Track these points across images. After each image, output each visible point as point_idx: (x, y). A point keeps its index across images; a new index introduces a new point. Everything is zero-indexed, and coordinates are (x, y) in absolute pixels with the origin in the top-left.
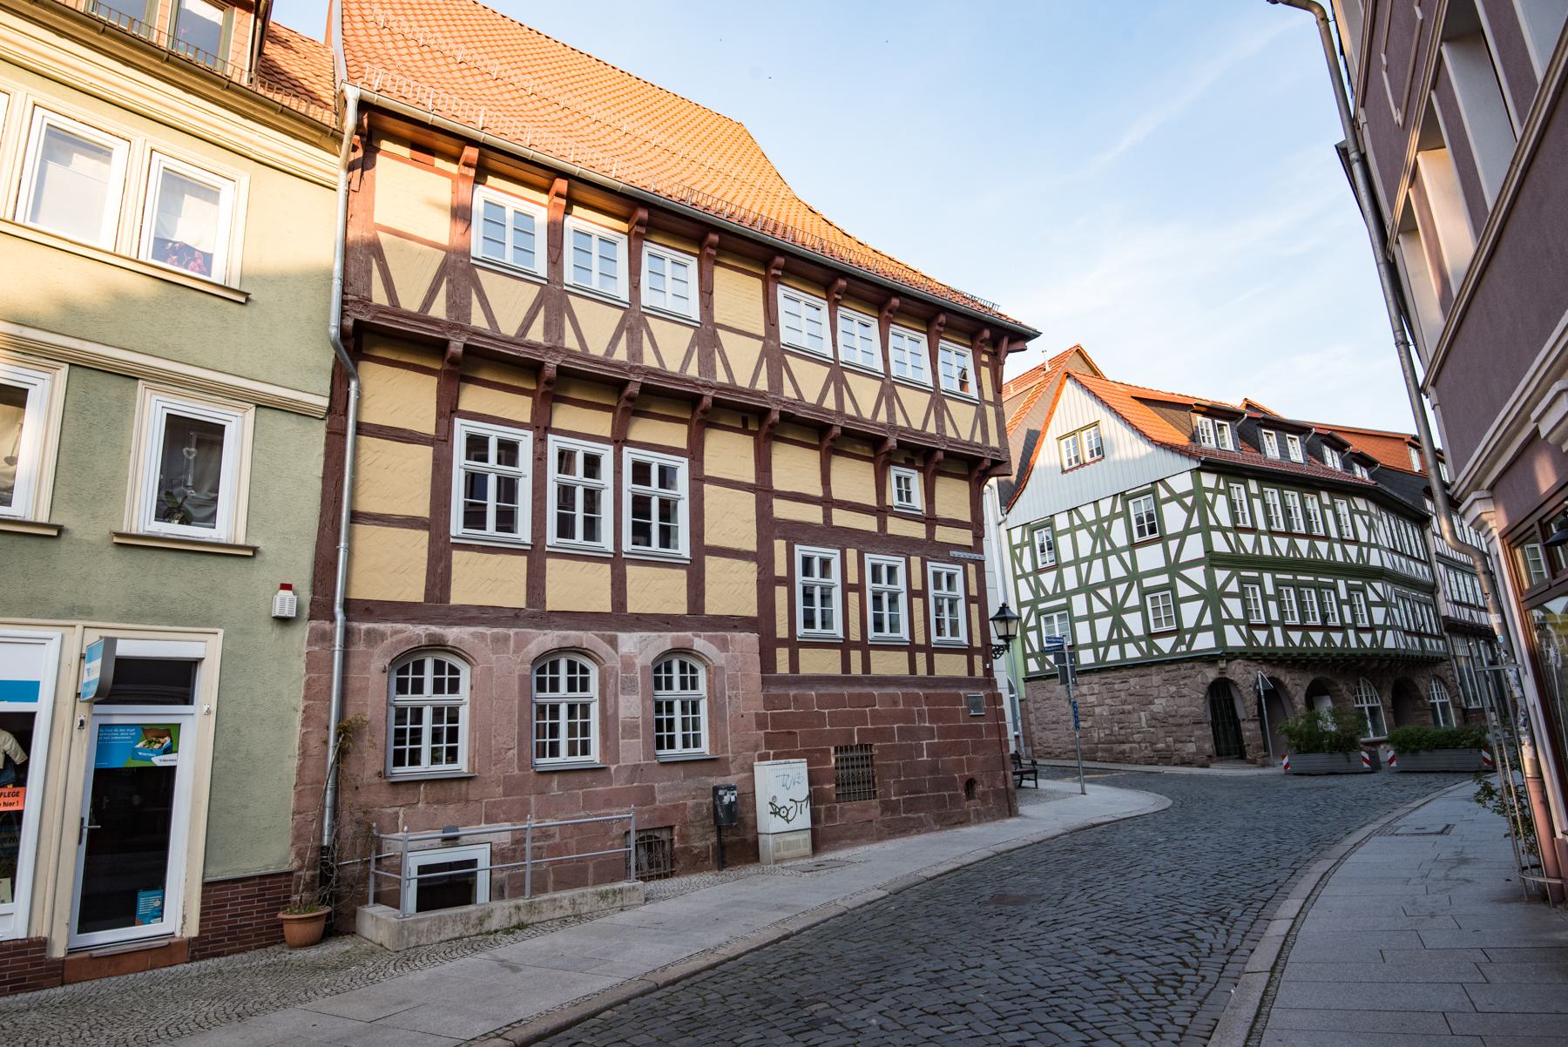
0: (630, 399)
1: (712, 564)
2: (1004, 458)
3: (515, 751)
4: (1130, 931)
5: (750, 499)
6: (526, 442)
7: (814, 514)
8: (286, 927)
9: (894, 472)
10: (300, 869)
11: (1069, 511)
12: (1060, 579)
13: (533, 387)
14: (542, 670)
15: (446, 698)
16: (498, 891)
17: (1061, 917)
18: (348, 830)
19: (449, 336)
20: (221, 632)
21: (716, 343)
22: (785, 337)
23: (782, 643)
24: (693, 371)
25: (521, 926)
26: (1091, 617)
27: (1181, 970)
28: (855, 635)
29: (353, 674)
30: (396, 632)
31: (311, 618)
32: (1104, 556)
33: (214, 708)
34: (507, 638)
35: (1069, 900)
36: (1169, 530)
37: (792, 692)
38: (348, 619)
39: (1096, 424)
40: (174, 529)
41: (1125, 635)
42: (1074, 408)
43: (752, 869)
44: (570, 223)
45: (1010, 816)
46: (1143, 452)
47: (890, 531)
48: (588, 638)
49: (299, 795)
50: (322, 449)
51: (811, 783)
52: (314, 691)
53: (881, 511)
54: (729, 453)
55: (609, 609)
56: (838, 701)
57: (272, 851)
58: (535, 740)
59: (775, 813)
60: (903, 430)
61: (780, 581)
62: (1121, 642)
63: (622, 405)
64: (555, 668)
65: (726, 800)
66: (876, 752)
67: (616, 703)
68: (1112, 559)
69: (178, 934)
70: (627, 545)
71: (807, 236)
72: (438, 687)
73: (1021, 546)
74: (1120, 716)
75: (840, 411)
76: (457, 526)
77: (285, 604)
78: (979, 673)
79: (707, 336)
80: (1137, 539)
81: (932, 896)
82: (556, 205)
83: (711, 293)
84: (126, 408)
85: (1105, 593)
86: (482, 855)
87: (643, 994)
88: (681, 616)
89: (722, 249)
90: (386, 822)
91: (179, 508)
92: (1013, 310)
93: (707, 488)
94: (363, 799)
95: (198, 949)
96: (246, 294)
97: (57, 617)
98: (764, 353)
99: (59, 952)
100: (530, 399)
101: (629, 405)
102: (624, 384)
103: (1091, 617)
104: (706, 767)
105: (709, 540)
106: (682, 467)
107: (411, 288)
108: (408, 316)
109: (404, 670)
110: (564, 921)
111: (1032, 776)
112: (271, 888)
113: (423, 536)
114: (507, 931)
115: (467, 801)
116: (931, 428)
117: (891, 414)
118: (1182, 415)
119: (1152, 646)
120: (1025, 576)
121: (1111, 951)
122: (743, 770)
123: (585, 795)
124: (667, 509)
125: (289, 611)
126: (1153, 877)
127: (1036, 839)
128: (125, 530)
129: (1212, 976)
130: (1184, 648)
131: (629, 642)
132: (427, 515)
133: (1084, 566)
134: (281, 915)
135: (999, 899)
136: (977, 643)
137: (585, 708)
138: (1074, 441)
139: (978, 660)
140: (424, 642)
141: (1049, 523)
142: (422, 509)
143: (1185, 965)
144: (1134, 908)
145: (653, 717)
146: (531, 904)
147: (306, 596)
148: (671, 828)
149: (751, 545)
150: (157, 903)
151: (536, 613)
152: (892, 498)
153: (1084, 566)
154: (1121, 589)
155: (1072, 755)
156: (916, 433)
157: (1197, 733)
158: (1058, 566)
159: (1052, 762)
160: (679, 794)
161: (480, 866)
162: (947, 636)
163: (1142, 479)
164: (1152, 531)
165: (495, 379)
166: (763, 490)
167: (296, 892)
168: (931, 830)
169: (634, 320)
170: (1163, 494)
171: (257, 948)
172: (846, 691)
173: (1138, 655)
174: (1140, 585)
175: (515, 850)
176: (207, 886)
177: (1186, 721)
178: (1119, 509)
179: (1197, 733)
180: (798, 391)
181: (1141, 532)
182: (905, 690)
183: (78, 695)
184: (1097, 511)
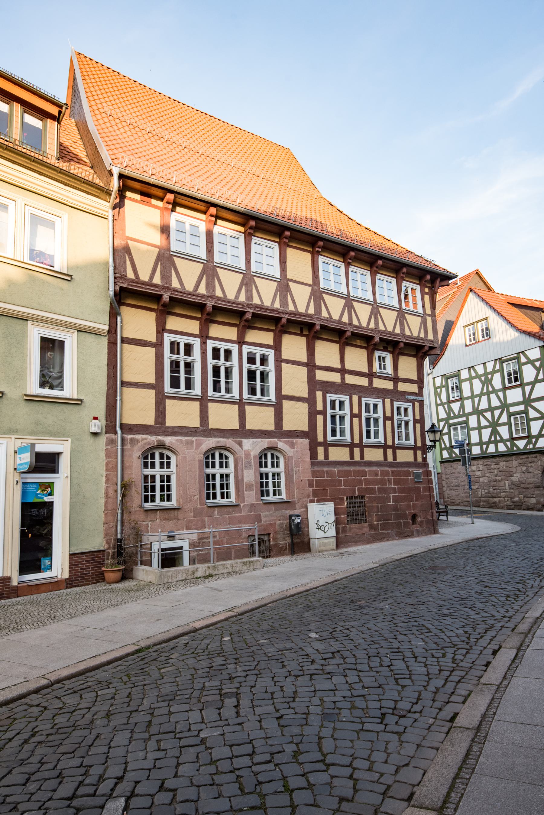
0: (247, 321)
1: (286, 404)
3: (198, 496)
4: (496, 579)
5: (304, 371)
6: (197, 343)
7: (336, 378)
8: (106, 575)
9: (377, 354)
10: (109, 548)
11: (469, 368)
12: (462, 407)
13: (200, 316)
14: (207, 458)
15: (165, 471)
16: (192, 561)
17: (463, 574)
18: (127, 532)
19: (162, 293)
20: (70, 440)
21: (288, 289)
22: (322, 284)
23: (320, 444)
24: (277, 305)
25: (210, 576)
26: (480, 428)
27: (518, 593)
28: (357, 440)
29: (126, 459)
30: (143, 439)
31: (106, 433)
32: (488, 394)
33: (69, 475)
35: (467, 568)
36: (526, 381)
37: (325, 469)
38: (122, 433)
39: (486, 319)
40: (46, 392)
41: (498, 438)
42: (474, 309)
43: (308, 555)
44: (217, 229)
45: (434, 533)
46: (513, 337)
48: (228, 442)
49: (106, 515)
50: (106, 351)
51: (335, 515)
52: (110, 467)
53: (371, 375)
54: (294, 346)
55: (238, 428)
57: (96, 541)
58: (143, 494)
60: (383, 332)
61: (320, 413)
62: (496, 442)
63: (242, 324)
64: (266, 456)
65: (296, 521)
66: (367, 500)
67: (243, 474)
68: (493, 396)
69: (59, 577)
70: (246, 395)
71: (332, 228)
72: (162, 465)
73: (440, 387)
74: (493, 483)
75: (350, 324)
76: (167, 388)
77: (96, 426)
78: (420, 460)
79: (284, 286)
80: (507, 385)
81: (401, 567)
82: (210, 221)
83: (285, 263)
84: (24, 334)
85: (488, 415)
86: (185, 544)
87: (282, 599)
88: (271, 431)
89: (291, 238)
90: (143, 528)
91: (48, 382)
92: (443, 261)
93: (284, 365)
94: (133, 517)
95: (70, 583)
96: (71, 276)
97: (4, 434)
98: (313, 293)
99: (15, 583)
100: (198, 322)
101: (246, 324)
102: (243, 313)
103: (480, 428)
104: (285, 505)
105: (151, 352)
106: (271, 355)
107: (145, 270)
108: (144, 283)
109: (146, 457)
110: (229, 574)
111: (445, 514)
112: (96, 557)
113: (153, 392)
114: (205, 577)
115: (178, 519)
116: (398, 331)
117: (377, 324)
118: (536, 314)
119: (513, 445)
120: (442, 404)
121: (487, 586)
122: (303, 507)
123: (230, 518)
124: (264, 376)
125: (98, 430)
126: (508, 560)
127: (449, 544)
128: (28, 393)
129: (531, 595)
130: (531, 446)
131: (248, 443)
132: (154, 382)
133: (476, 400)
134: (103, 569)
135: (433, 568)
136: (419, 444)
137: (227, 476)
138: (473, 328)
139: (419, 453)
141: (457, 375)
142: (151, 379)
143: (520, 591)
144: (498, 571)
145: (259, 481)
146: (214, 566)
147: (104, 422)
148: (269, 534)
149: (305, 395)
150: (49, 563)
151: (203, 429)
152: (376, 368)
153: (476, 400)
154: (497, 413)
155: (466, 504)
156: (390, 333)
157: (537, 492)
158: (461, 399)
159: (455, 508)
160: (274, 518)
161: (184, 549)
162: (404, 441)
163: (512, 352)
164: (516, 379)
165: (182, 313)
166: (311, 365)
167: (108, 559)
168: (394, 539)
169: (248, 280)
170: (523, 359)
171: (92, 583)
172: (352, 468)
173: (505, 449)
174: (508, 410)
175: (199, 543)
176: (71, 555)
177: (531, 486)
178: (497, 367)
179: (537, 492)
180: (329, 313)
181: (510, 381)
182: (382, 468)
183: (15, 469)
184: (485, 368)
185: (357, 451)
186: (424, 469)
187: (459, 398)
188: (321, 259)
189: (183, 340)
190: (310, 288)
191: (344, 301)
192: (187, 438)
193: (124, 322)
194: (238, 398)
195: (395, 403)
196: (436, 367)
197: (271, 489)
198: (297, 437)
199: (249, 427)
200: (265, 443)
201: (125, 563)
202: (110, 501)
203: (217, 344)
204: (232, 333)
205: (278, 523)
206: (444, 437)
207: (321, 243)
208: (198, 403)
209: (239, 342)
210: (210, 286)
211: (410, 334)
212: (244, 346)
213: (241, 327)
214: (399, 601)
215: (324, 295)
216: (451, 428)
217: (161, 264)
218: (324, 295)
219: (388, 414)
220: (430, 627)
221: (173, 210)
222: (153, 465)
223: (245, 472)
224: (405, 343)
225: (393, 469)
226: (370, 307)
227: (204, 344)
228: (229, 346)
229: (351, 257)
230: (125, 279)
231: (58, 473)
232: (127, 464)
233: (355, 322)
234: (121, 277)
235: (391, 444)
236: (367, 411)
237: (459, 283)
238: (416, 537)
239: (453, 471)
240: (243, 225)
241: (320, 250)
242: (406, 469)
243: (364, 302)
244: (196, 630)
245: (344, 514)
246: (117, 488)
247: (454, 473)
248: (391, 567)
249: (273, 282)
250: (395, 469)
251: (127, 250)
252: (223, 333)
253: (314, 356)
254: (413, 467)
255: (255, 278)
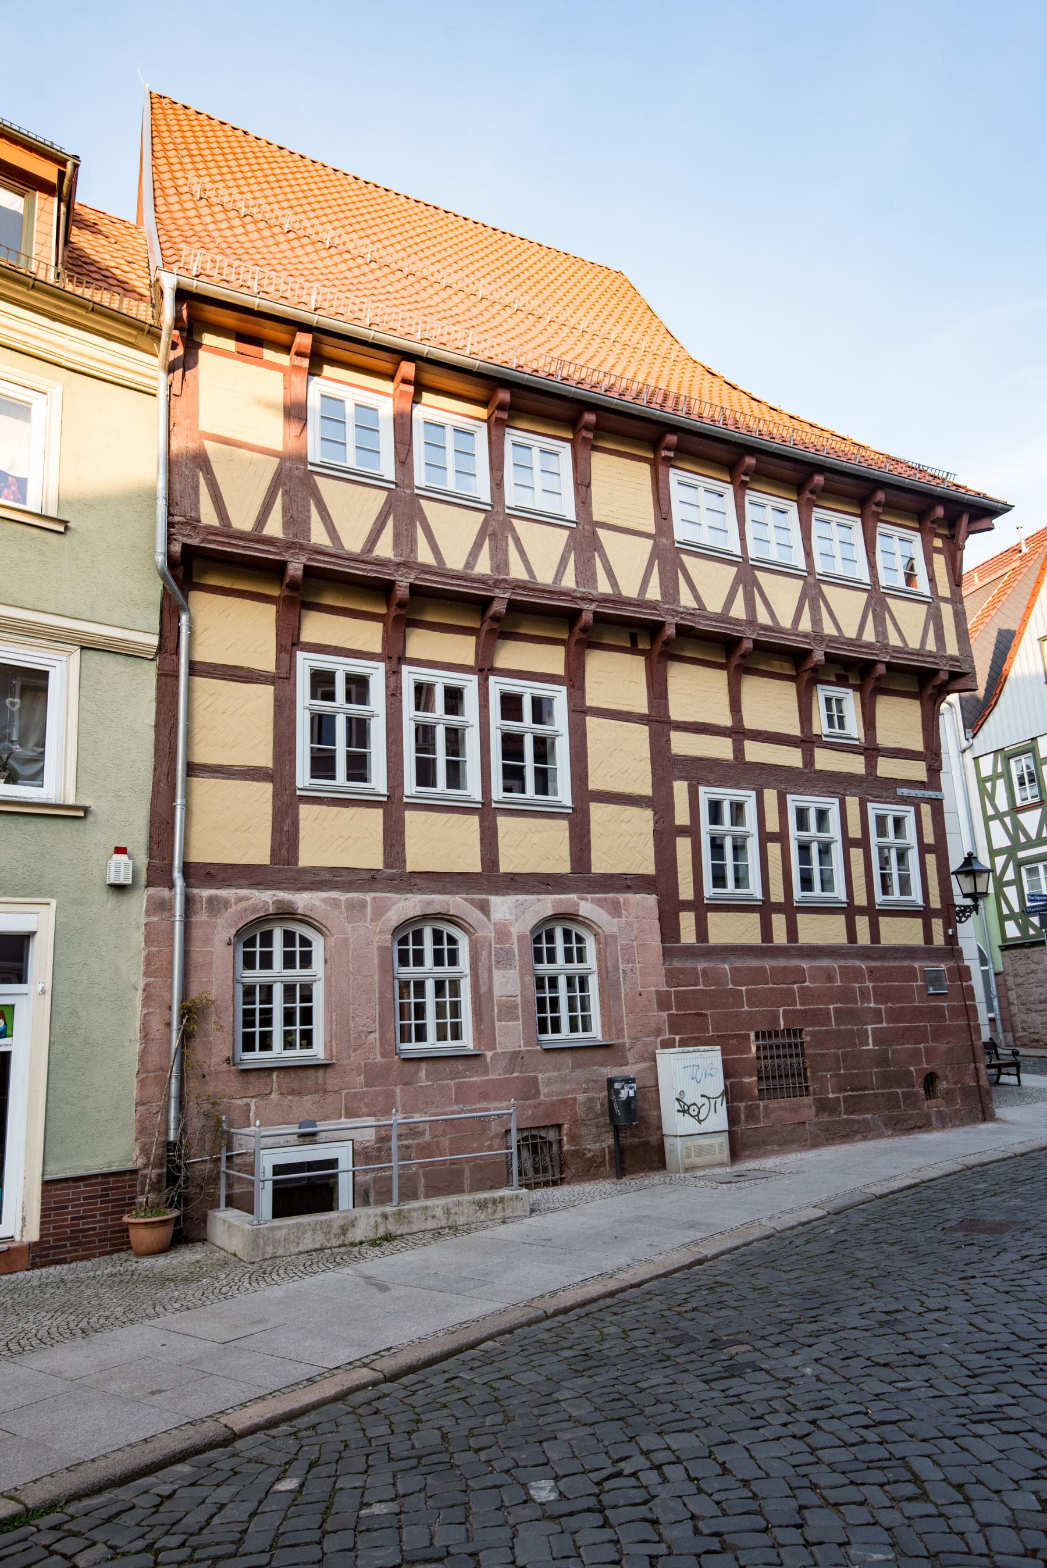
0: (496, 618)
1: (598, 812)
2: (965, 668)
3: (377, 1035)
6: (377, 675)
7: (721, 749)
9: (822, 692)
10: (146, 1166)
14: (404, 941)
15: (298, 974)
16: (362, 1197)
18: (196, 1124)
19: (286, 557)
20: (53, 902)
21: (596, 546)
22: (681, 532)
23: (687, 906)
24: (569, 581)
25: (389, 1238)
28: (777, 895)
29: (196, 947)
30: (240, 900)
31: (149, 884)
33: (48, 987)
34: (363, 904)
37: (701, 965)
38: (188, 885)
43: (657, 1178)
44: (420, 413)
47: (818, 766)
48: (455, 903)
49: (142, 1083)
50: (152, 694)
51: (726, 1076)
53: (807, 742)
54: (616, 678)
55: (478, 869)
56: (758, 976)
57: (116, 1148)
59: (684, 1112)
60: (832, 639)
61: (682, 831)
63: (486, 627)
64: (267, 939)
65: (623, 1095)
66: (807, 1039)
69: (17, 1238)
70: (497, 793)
71: (706, 407)
72: (289, 961)
75: (752, 621)
76: (303, 776)
77: (120, 869)
78: (939, 940)
79: (584, 538)
82: (403, 394)
83: (589, 485)
86: (343, 1154)
88: (562, 876)
89: (600, 430)
90: (236, 1114)
92: (974, 479)
93: (591, 721)
94: (210, 1088)
95: (39, 1255)
96: (65, 523)
98: (656, 554)
100: (381, 625)
101: (495, 626)
104: (597, 1055)
105: (594, 784)
106: (560, 698)
107: (243, 504)
108: (241, 536)
109: (251, 942)
110: (437, 1233)
112: (113, 1188)
114: (374, 1243)
115: (325, 1091)
117: (816, 621)
120: (999, 816)
122: (644, 1060)
123: (458, 1087)
124: (543, 748)
125: (125, 879)
127: (1019, 1149)
131: (503, 907)
132: (270, 765)
134: (126, 1219)
135: (970, 1225)
136: (936, 903)
139: (937, 924)
140: (271, 910)
142: (265, 758)
145: (534, 994)
146: (399, 1213)
147: (142, 860)
148: (559, 1127)
151: (395, 875)
152: (820, 725)
156: (850, 642)
160: (565, 1086)
162: (896, 895)
166: (658, 721)
167: (142, 1193)
168: (881, 1136)
169: (497, 525)
171: (101, 1254)
172: (768, 964)
175: (379, 1149)
176: (46, 1184)
180: (697, 598)
182: (843, 963)
185: (779, 922)
186: (952, 964)
187: (1037, 800)
188: (674, 476)
189: (341, 667)
190: (651, 542)
191: (735, 569)
192: (350, 895)
193: (199, 628)
194: (479, 799)
195: (870, 805)
196: (980, 733)
197: (564, 1014)
198: (628, 888)
199: (506, 866)
200: (546, 904)
201: (184, 1200)
202: (153, 1048)
203: (426, 675)
204: (462, 649)
205: (581, 1097)
206: (1006, 890)
207: (672, 439)
208: (380, 811)
209: (481, 670)
210: (404, 539)
211: (900, 644)
212: (492, 679)
213: (483, 634)
214: (850, 1347)
215: (684, 558)
216: (1023, 870)
217: (285, 493)
218: (684, 558)
219: (855, 832)
220: (924, 1468)
221: (314, 370)
222: (267, 962)
223: (497, 975)
224: (887, 663)
225: (872, 964)
226: (801, 583)
227: (393, 674)
228: (455, 679)
229: (748, 468)
230: (195, 527)
231: (26, 983)
232: (197, 958)
233: (763, 617)
234: (187, 523)
235: (865, 903)
236: (802, 825)
237: (1025, 550)
238: (937, 1129)
239: (1033, 967)
240: (484, 404)
241: (671, 454)
242: (905, 963)
243: (784, 571)
244: (228, 1439)
245: (750, 1075)
246: (171, 1016)
247: (1033, 972)
248: (858, 1219)
249: (558, 530)
250: (878, 964)
251: (201, 461)
252: (441, 650)
253: (666, 698)
254: (923, 959)
255: (514, 521)
